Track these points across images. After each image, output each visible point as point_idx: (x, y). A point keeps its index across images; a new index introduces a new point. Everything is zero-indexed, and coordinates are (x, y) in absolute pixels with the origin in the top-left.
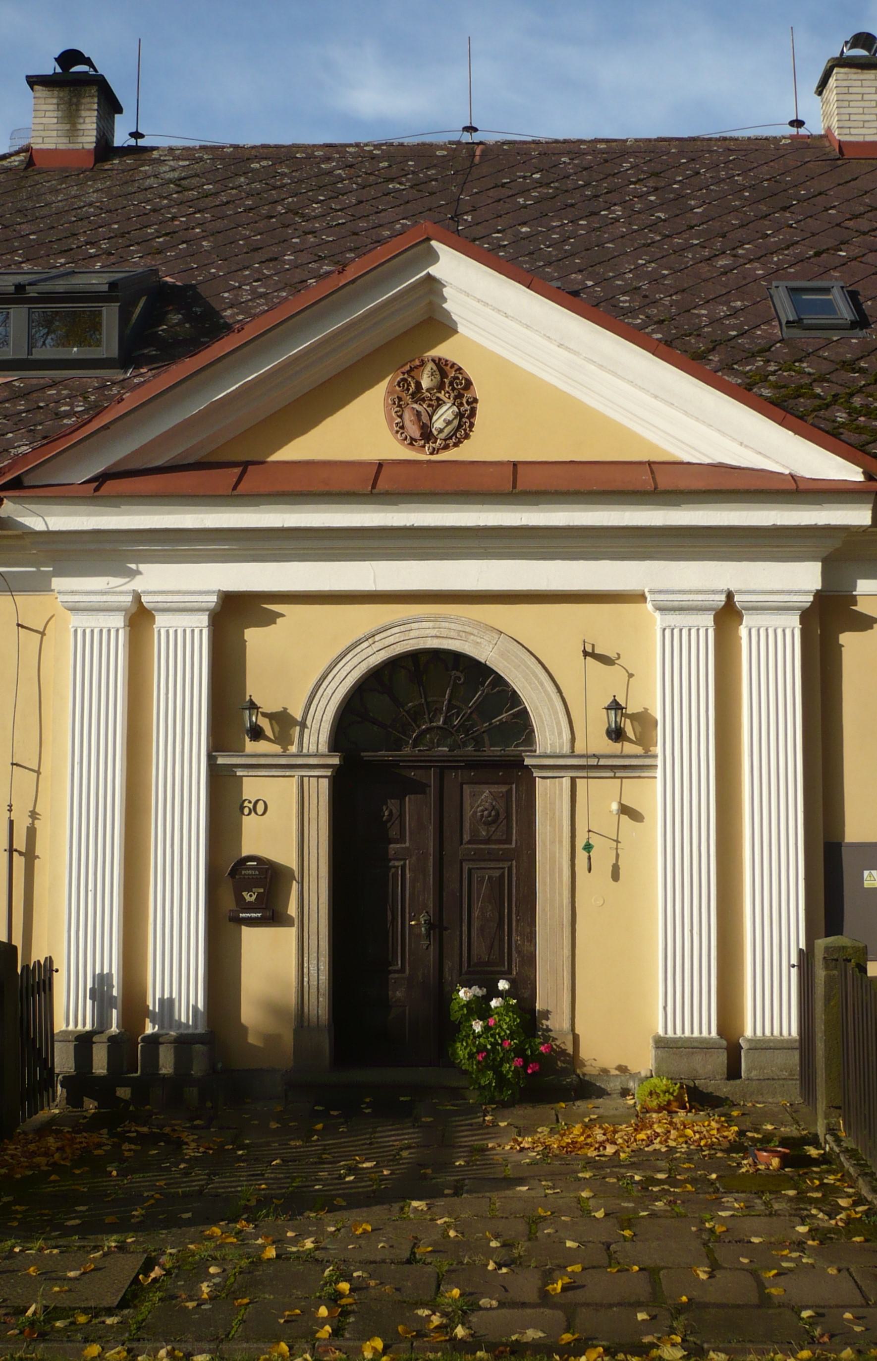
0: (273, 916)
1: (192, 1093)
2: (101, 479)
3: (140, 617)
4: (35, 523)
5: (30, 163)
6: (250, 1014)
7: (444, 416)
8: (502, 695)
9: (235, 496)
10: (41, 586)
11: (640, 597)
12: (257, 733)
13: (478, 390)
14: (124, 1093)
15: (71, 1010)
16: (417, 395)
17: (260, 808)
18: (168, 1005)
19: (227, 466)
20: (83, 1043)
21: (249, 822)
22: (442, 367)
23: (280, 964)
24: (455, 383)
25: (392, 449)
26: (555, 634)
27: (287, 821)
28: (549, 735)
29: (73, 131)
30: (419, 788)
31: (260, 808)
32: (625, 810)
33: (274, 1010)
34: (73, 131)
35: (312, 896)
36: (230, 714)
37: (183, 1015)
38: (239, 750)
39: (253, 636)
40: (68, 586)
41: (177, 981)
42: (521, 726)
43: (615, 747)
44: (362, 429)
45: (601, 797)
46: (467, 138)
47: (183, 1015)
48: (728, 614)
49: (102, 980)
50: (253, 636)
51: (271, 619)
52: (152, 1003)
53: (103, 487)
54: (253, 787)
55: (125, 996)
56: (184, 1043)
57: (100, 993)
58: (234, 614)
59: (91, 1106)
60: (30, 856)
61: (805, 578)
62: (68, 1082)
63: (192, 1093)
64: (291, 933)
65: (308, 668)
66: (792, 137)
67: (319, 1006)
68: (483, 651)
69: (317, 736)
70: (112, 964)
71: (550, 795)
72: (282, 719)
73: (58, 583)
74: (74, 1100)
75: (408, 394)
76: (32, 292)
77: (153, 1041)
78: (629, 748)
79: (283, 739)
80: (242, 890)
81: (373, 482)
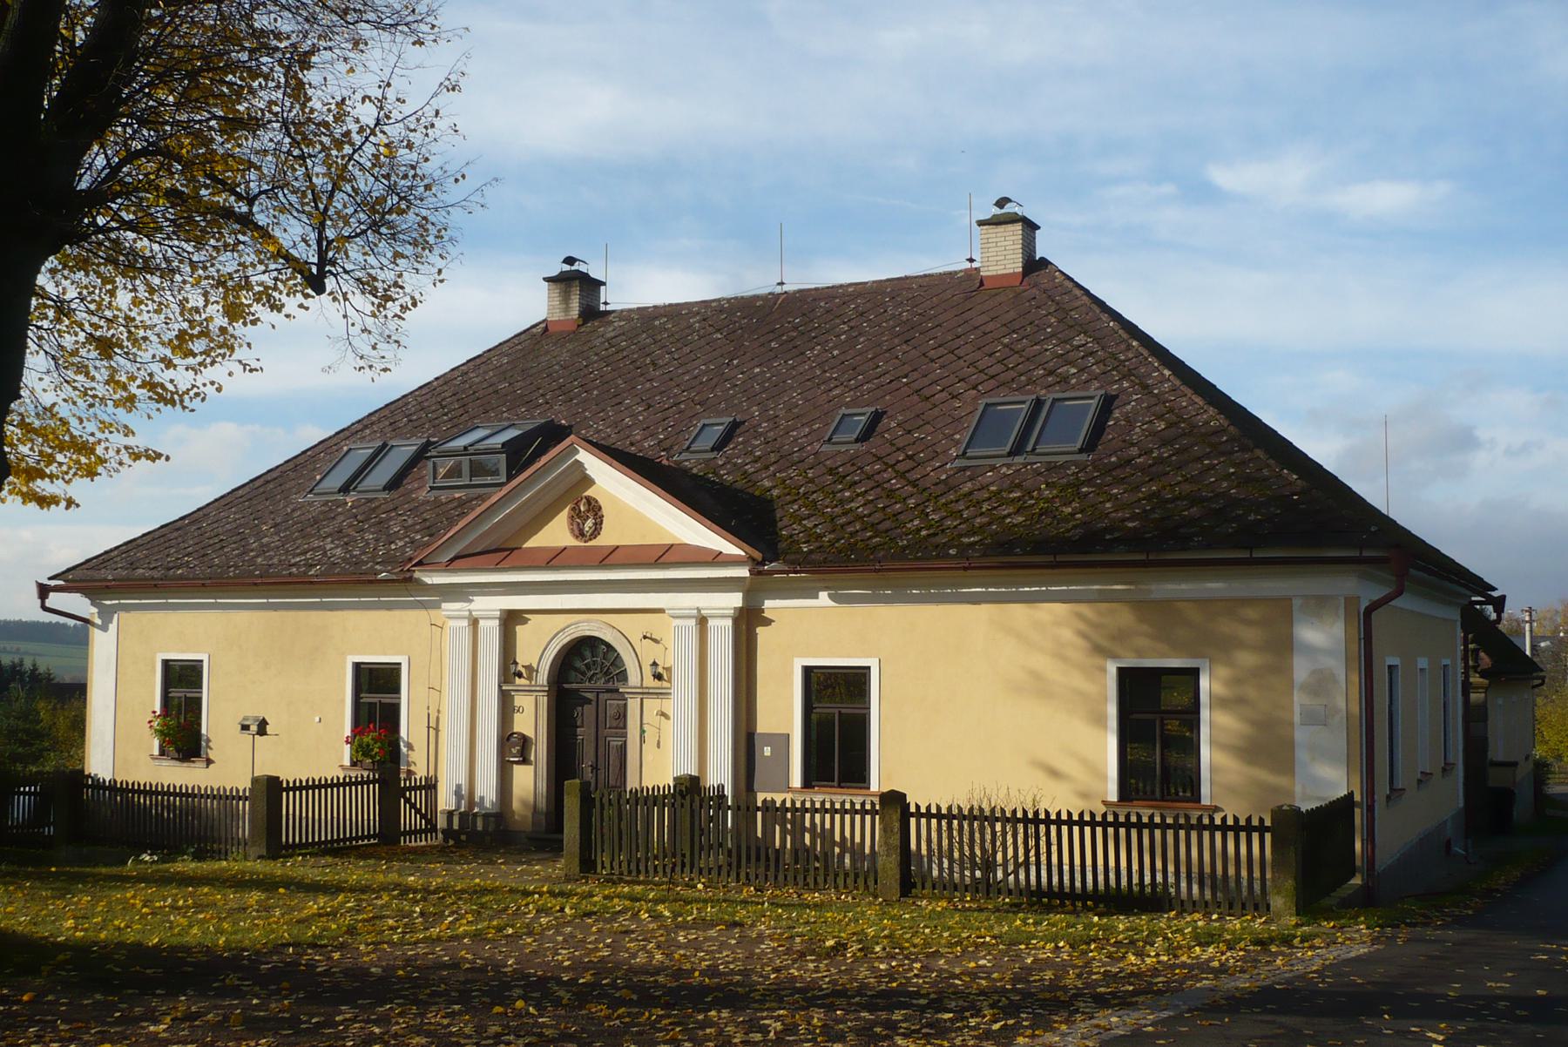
0: (525, 761)
1: (488, 838)
2: (452, 560)
3: (474, 623)
4: (428, 580)
5: (546, 329)
6: (516, 805)
7: (589, 523)
8: (617, 660)
9: (497, 568)
10: (437, 606)
11: (661, 611)
12: (520, 675)
13: (605, 511)
14: (463, 837)
15: (445, 800)
16: (579, 514)
17: (520, 710)
18: (482, 798)
19: (502, 551)
20: (450, 814)
21: (517, 716)
22: (589, 500)
23: (528, 781)
24: (594, 508)
25: (569, 540)
26: (634, 627)
27: (531, 718)
28: (633, 678)
29: (567, 310)
30: (589, 701)
31: (520, 710)
32: (663, 714)
33: (524, 803)
34: (567, 310)
35: (540, 751)
36: (509, 669)
37: (488, 804)
38: (512, 683)
39: (519, 629)
40: (450, 607)
41: (487, 790)
42: (623, 676)
43: (657, 683)
44: (556, 533)
45: (652, 705)
46: (778, 290)
47: (488, 804)
48: (702, 621)
49: (459, 787)
50: (519, 629)
51: (525, 621)
52: (477, 799)
53: (451, 565)
54: (520, 700)
55: (466, 794)
56: (486, 816)
57: (458, 793)
58: (511, 620)
59: (451, 842)
60: (437, 730)
61: (735, 600)
62: (443, 832)
63: (488, 838)
64: (532, 768)
65: (538, 647)
66: (966, 270)
67: (542, 804)
68: (607, 636)
69: (543, 677)
70: (463, 780)
71: (633, 705)
72: (529, 668)
73: (444, 605)
74: (446, 840)
75: (577, 518)
76: (471, 449)
77: (475, 815)
78: (665, 684)
79: (530, 678)
80: (513, 747)
81: (555, 558)
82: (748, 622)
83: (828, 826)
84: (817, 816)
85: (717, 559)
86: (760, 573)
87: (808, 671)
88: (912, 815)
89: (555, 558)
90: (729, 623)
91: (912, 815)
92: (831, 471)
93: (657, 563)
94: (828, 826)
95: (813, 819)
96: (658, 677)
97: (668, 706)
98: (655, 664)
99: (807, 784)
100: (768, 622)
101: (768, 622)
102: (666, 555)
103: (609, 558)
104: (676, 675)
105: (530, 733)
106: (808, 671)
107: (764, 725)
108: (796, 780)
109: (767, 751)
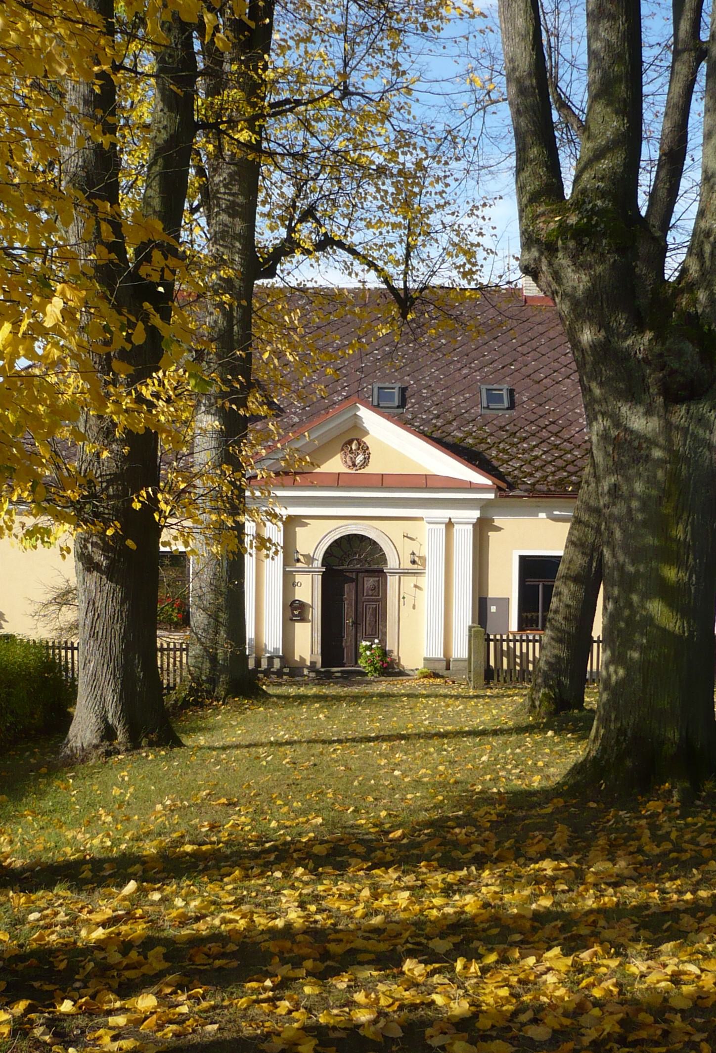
0: (303, 619)
9: (294, 486)
11: (421, 519)
13: (371, 450)
28: (392, 563)
35: (316, 613)
39: (299, 530)
42: (383, 559)
44: (336, 464)
45: (408, 582)
48: (450, 524)
50: (299, 530)
54: (299, 578)
61: (476, 514)
68: (372, 535)
81: (337, 481)
82: (482, 529)
83: (524, 650)
84: (498, 643)
85: (471, 487)
86: (501, 496)
87: (523, 559)
88: (595, 642)
89: (337, 481)
90: (471, 527)
91: (595, 642)
92: (502, 428)
93: (426, 488)
94: (524, 650)
95: (508, 645)
96: (414, 562)
97: (423, 581)
98: (413, 554)
99: (521, 628)
100: (498, 529)
101: (498, 529)
102: (427, 482)
103: (383, 481)
104: (429, 563)
105: (307, 600)
106: (523, 559)
107: (493, 592)
108: (514, 626)
109: (493, 609)
